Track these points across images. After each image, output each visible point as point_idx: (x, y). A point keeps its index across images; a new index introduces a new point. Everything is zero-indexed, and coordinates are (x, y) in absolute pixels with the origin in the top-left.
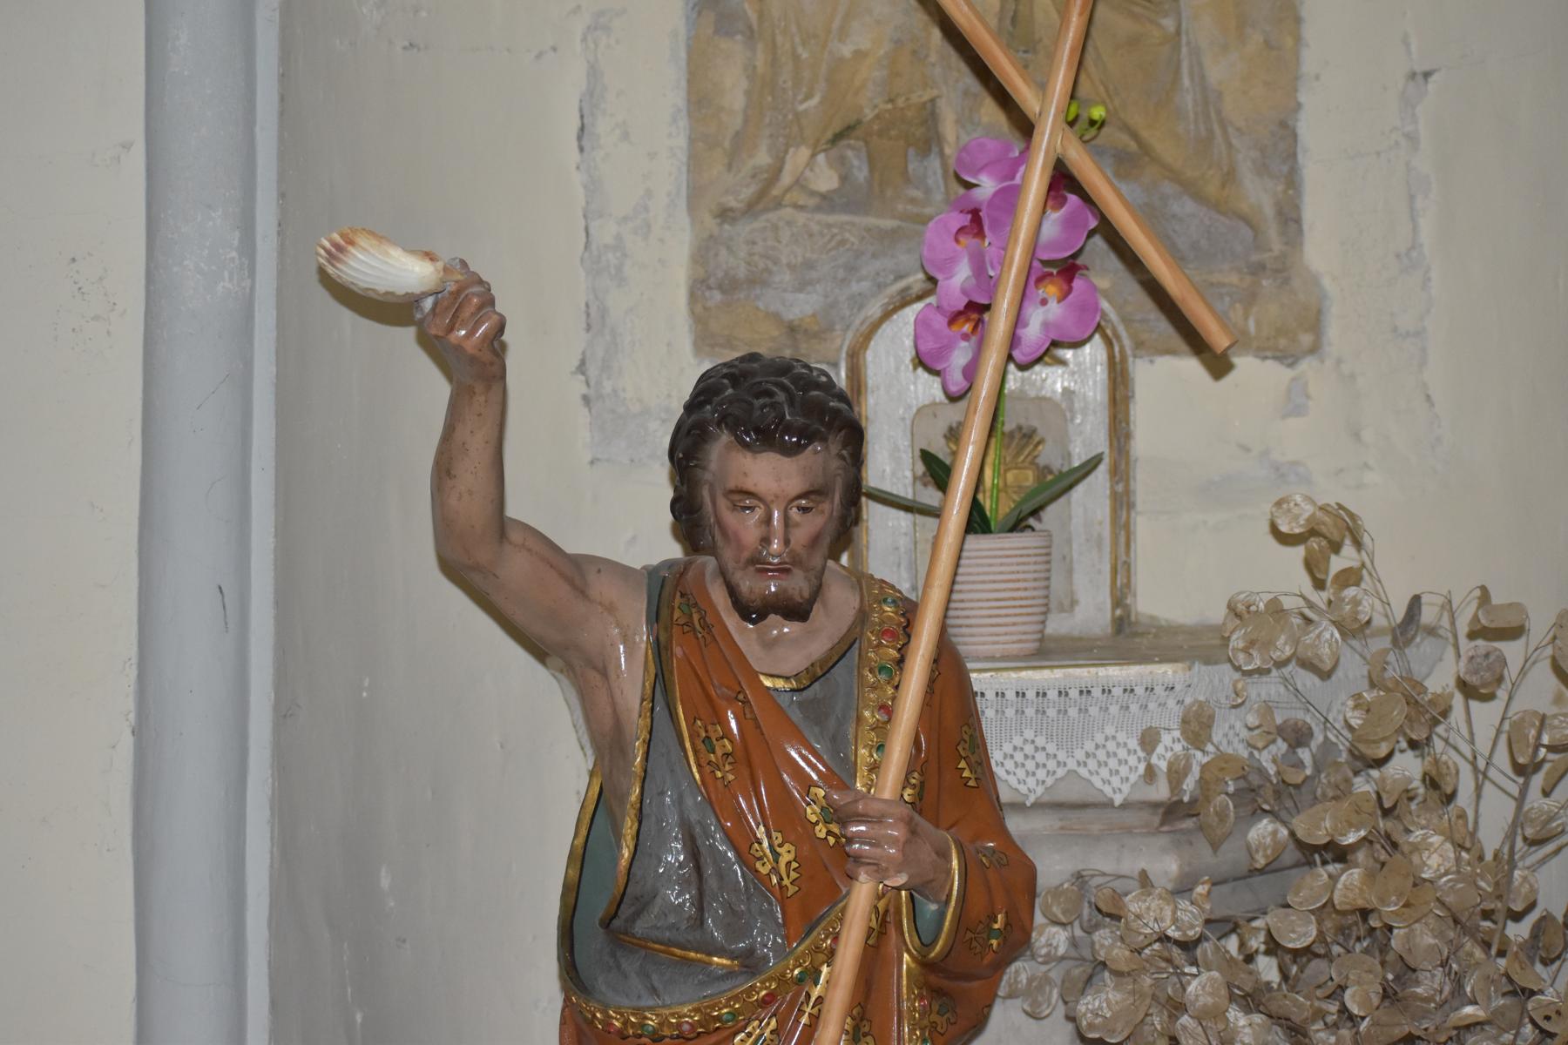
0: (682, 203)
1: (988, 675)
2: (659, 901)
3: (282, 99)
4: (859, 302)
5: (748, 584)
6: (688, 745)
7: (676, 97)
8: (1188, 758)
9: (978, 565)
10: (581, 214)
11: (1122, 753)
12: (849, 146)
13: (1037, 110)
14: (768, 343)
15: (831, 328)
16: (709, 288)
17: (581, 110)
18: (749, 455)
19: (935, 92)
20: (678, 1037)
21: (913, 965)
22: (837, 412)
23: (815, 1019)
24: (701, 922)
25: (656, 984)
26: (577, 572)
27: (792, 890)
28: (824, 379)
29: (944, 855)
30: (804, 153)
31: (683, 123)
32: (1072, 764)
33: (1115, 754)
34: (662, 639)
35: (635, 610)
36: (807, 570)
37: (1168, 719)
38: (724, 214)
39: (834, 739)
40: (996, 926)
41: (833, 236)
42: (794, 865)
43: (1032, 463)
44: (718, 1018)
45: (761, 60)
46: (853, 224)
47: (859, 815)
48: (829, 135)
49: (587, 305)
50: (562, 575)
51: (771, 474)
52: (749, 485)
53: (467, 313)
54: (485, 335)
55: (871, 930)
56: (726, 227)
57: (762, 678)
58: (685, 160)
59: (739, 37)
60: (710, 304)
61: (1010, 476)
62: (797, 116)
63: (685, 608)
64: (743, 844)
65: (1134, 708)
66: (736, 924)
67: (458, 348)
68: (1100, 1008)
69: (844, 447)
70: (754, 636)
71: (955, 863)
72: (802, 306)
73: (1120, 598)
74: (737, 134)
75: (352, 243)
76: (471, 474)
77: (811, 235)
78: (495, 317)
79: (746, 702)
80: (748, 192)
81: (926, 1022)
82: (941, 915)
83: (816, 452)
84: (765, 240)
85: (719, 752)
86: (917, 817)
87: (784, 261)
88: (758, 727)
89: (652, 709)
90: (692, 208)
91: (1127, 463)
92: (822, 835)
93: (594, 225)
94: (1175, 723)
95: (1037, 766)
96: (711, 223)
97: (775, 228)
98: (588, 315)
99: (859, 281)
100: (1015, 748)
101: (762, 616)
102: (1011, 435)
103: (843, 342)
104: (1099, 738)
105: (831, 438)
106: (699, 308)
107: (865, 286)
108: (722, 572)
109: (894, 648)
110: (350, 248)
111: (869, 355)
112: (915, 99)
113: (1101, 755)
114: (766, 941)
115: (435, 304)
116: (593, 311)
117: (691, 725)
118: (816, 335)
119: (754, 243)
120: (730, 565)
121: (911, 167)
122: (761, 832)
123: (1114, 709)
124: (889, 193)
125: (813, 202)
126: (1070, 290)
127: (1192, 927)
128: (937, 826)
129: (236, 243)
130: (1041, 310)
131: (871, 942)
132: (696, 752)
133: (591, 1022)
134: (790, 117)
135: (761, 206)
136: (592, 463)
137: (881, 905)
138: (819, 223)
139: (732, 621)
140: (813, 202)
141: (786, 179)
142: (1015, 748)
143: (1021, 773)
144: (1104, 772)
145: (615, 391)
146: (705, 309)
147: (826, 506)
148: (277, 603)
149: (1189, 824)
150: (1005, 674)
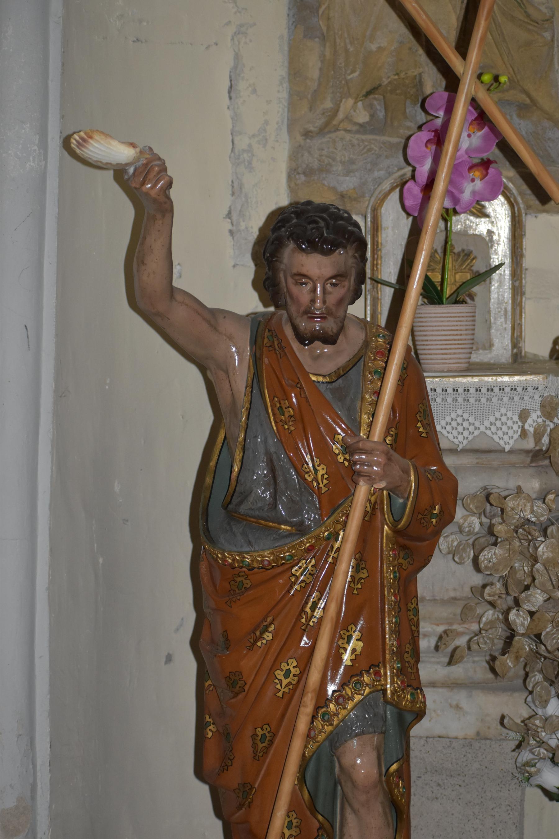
0: (285, 128)
1: (438, 379)
2: (253, 495)
3: (63, 65)
4: (379, 182)
5: (303, 325)
6: (270, 411)
7: (283, 72)
8: (545, 426)
9: (435, 321)
10: (230, 133)
11: (510, 423)
12: (375, 99)
13: (462, 72)
14: (321, 197)
15: (363, 196)
16: (298, 173)
17: (230, 77)
18: (304, 255)
19: (421, 70)
20: (262, 568)
21: (389, 532)
22: (352, 233)
23: (335, 559)
24: (274, 506)
25: (251, 540)
26: (214, 317)
27: (324, 490)
28: (346, 215)
29: (408, 473)
30: (350, 101)
31: (286, 85)
32: (482, 429)
33: (506, 424)
34: (258, 355)
35: (244, 336)
36: (335, 318)
37: (533, 403)
38: (307, 134)
39: (349, 409)
40: (435, 512)
41: (365, 147)
42: (326, 476)
43: (470, 269)
44: (283, 558)
45: (328, 53)
46: (376, 140)
47: (361, 450)
48: (364, 92)
49: (232, 182)
50: (204, 319)
51: (316, 265)
52: (304, 271)
53: (152, 175)
54: (161, 187)
55: (366, 513)
56: (308, 141)
57: (311, 375)
58: (286, 104)
59: (317, 40)
60: (299, 182)
61: (457, 276)
62: (347, 82)
63: (270, 338)
64: (298, 465)
65: (516, 399)
66: (295, 508)
67: (147, 194)
68: (492, 558)
69: (356, 252)
70: (307, 353)
71: (413, 478)
72: (348, 184)
73: (516, 342)
74: (315, 91)
75: (91, 137)
76: (154, 263)
77: (353, 146)
78: (167, 178)
79: (301, 388)
80: (320, 122)
81: (396, 563)
82: (405, 505)
83: (340, 254)
84: (328, 148)
85: (287, 415)
86: (392, 452)
87: (339, 159)
88: (308, 401)
89: (252, 392)
90: (290, 131)
91: (521, 271)
92: (341, 461)
93: (236, 139)
94: (538, 407)
95: (464, 429)
96: (299, 138)
97: (334, 142)
98: (233, 187)
99: (379, 170)
100: (452, 419)
101: (311, 342)
102: (459, 254)
103: (367, 203)
104: (498, 415)
105: (349, 246)
106: (293, 185)
107: (382, 173)
108: (291, 320)
109: (382, 361)
110: (90, 140)
111: (383, 210)
112: (410, 73)
113: (498, 424)
114: (309, 517)
115: (135, 170)
116: (236, 185)
117: (272, 401)
118: (355, 200)
119: (323, 150)
120: (294, 314)
121: (407, 111)
122: (308, 458)
123: (505, 399)
124: (396, 124)
125: (355, 128)
126: (487, 173)
127: (543, 515)
128: (404, 456)
129: (37, 142)
130: (472, 184)
131: (366, 519)
132: (274, 415)
133: (216, 560)
134: (343, 82)
135: (326, 130)
136: (234, 266)
137: (373, 499)
138: (358, 139)
139: (295, 345)
140: (355, 128)
141: (341, 115)
142: (452, 419)
143: (455, 433)
144: (500, 433)
145: (247, 228)
146: (296, 184)
147: (346, 283)
148: (57, 335)
149: (547, 462)
150: (447, 379)
